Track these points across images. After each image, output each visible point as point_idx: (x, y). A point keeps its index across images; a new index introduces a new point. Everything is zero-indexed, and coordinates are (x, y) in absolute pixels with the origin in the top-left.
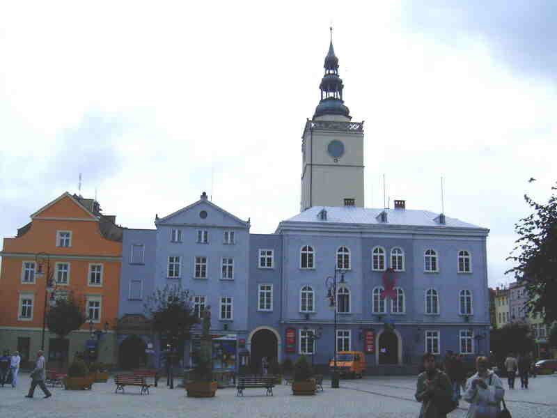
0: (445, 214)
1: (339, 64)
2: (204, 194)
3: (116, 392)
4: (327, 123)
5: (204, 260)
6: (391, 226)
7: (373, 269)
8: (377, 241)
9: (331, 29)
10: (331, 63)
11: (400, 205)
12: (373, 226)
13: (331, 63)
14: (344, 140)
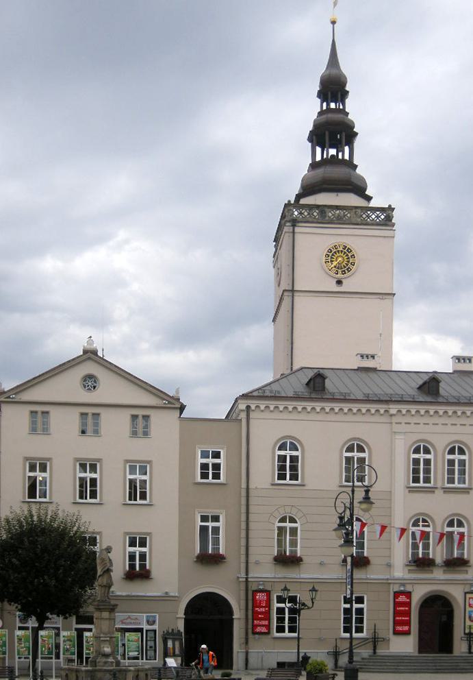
4: (322, 209)
7: (199, 479)
9: (333, 23)
10: (333, 88)
13: (333, 88)
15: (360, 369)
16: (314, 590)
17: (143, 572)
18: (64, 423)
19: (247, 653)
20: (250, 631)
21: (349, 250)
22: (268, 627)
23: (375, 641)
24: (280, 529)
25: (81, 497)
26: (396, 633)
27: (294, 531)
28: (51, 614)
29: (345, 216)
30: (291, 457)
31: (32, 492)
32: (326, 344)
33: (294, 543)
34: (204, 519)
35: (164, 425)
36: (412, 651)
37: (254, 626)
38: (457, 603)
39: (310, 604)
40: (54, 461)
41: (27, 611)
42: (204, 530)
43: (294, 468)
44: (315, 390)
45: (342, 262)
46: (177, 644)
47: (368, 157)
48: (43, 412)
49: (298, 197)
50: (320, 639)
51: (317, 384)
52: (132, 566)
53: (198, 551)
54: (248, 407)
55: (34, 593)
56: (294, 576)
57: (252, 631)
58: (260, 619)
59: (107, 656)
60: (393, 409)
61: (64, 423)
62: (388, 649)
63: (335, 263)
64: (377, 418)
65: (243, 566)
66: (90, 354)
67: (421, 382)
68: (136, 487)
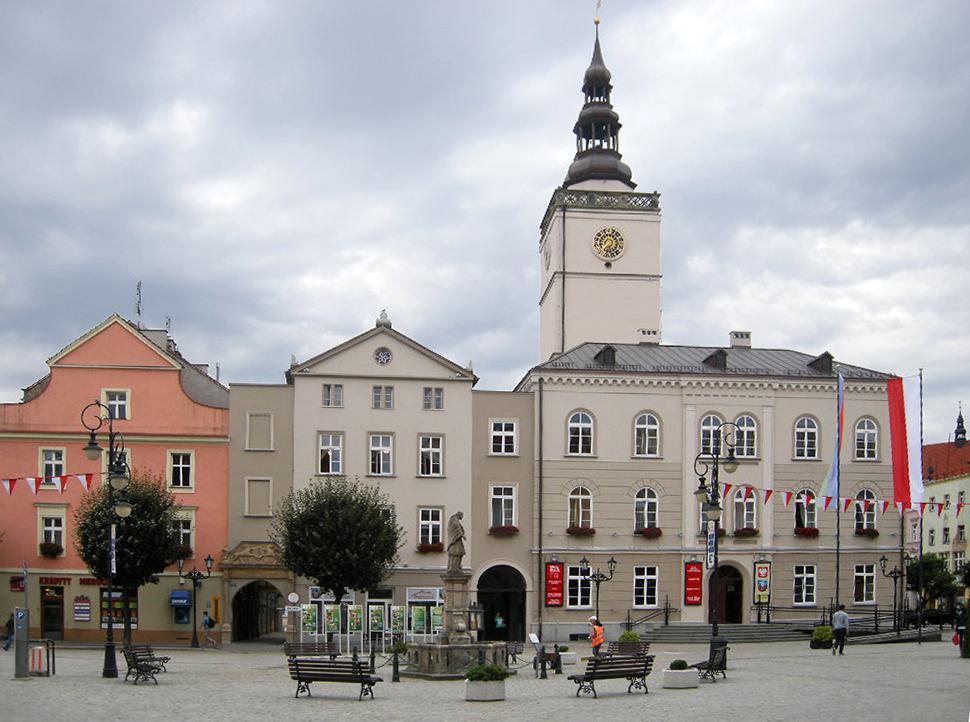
1: (611, 83)
3: (578, 696)
4: (591, 194)
5: (436, 443)
7: (492, 453)
9: (597, 23)
10: (597, 84)
13: (597, 84)
15: (642, 344)
16: (612, 561)
17: (436, 545)
18: (358, 396)
19: (540, 626)
20: (543, 604)
21: (618, 234)
22: (561, 599)
23: (667, 612)
24: (573, 502)
25: (374, 471)
26: (688, 603)
27: (586, 503)
28: (350, 588)
30: (507, 437)
31: (325, 466)
32: (604, 317)
33: (586, 515)
34: (497, 491)
35: (457, 398)
36: (702, 621)
37: (548, 599)
38: (747, 573)
39: (608, 575)
40: (347, 436)
41: (325, 585)
42: (496, 503)
43: (586, 441)
44: (604, 363)
45: (611, 245)
46: (479, 617)
47: (630, 147)
48: (336, 386)
49: (566, 184)
50: (612, 610)
51: (606, 358)
52: (425, 539)
53: (491, 524)
54: (541, 380)
55: (335, 567)
56: (587, 548)
57: (545, 603)
58: (554, 592)
59: (461, 631)
60: (684, 381)
61: (358, 396)
62: (680, 619)
63: (604, 247)
64: (667, 390)
65: (536, 538)
66: (384, 327)
67: (704, 357)
68: (428, 461)
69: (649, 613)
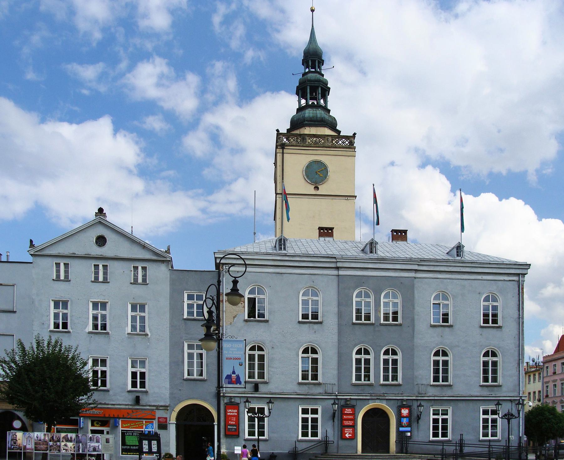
0: (463, 243)
2: (101, 210)
6: (383, 260)
8: (360, 281)
9: (313, 11)
11: (399, 235)
12: (355, 260)
14: (328, 158)
18: (82, 271)
29: (320, 141)
45: (316, 174)
47: (336, 105)
69: (313, 444)
